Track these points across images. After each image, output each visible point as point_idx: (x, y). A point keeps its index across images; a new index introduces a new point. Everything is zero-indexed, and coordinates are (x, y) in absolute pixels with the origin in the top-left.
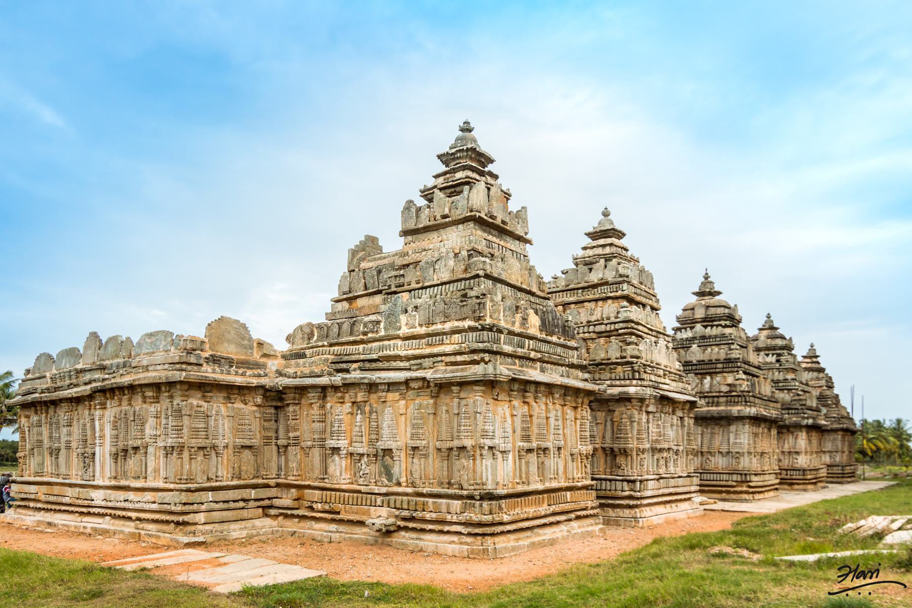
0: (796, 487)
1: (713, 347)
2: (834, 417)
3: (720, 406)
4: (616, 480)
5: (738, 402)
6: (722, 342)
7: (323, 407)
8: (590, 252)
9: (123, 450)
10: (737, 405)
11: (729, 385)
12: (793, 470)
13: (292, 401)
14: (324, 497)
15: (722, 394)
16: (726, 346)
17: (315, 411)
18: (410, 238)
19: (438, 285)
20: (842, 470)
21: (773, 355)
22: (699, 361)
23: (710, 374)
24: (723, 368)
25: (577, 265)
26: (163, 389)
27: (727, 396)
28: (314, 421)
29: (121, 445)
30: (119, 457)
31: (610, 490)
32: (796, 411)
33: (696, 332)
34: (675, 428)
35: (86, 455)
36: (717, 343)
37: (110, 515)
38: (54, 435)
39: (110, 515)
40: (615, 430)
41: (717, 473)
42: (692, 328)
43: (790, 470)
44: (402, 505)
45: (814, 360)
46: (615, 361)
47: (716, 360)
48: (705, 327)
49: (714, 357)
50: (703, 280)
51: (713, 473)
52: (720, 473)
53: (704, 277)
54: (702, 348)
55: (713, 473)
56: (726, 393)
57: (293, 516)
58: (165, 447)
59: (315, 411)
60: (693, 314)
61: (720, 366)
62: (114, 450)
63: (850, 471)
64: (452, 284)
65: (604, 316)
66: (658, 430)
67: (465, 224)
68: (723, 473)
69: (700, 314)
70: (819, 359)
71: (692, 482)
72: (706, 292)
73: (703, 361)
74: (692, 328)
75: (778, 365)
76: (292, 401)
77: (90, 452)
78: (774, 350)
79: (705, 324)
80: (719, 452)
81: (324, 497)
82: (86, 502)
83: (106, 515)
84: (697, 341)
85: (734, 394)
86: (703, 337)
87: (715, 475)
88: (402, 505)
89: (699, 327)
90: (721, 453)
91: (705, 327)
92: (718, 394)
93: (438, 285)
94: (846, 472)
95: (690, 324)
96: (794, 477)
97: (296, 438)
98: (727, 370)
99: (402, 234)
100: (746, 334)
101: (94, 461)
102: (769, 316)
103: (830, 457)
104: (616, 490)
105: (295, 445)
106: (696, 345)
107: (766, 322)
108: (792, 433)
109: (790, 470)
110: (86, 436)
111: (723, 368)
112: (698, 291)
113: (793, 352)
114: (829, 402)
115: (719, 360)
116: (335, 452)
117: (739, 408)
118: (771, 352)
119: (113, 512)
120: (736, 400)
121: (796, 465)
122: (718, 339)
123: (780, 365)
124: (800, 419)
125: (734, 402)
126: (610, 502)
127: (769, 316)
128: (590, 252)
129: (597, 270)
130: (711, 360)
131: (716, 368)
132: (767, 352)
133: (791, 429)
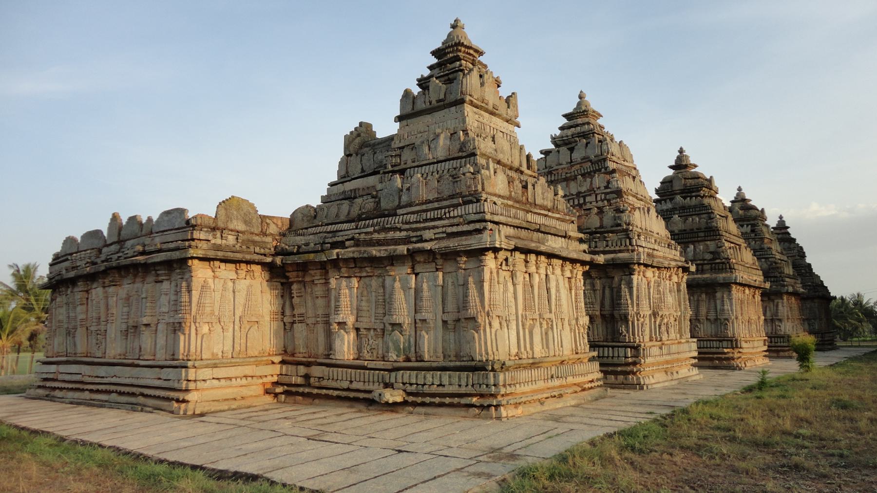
0: (782, 354)
1: (694, 217)
2: (810, 286)
3: (705, 274)
4: (619, 347)
5: (722, 269)
6: (701, 212)
7: (327, 283)
8: (569, 132)
9: (133, 326)
10: (722, 273)
11: (711, 253)
12: (778, 337)
13: (296, 279)
14: (331, 373)
15: (706, 262)
16: (706, 215)
17: (319, 290)
18: (404, 122)
19: (434, 163)
20: (822, 337)
21: (747, 225)
22: (680, 231)
23: (693, 243)
24: (705, 236)
25: (556, 145)
26: (175, 265)
27: (711, 264)
28: (317, 297)
29: (131, 323)
30: (129, 335)
31: (608, 357)
32: (775, 279)
33: (676, 203)
34: (673, 294)
35: (98, 332)
36: (697, 213)
37: (116, 392)
38: (71, 315)
39: (116, 392)
40: (615, 297)
41: (706, 341)
42: (671, 200)
43: (774, 337)
44: (410, 379)
45: (783, 231)
46: (609, 229)
47: (697, 229)
48: (685, 198)
49: (695, 227)
50: (679, 154)
51: (703, 341)
52: (710, 340)
53: (679, 151)
54: (683, 218)
55: (703, 341)
56: (710, 260)
57: (297, 394)
58: (174, 323)
59: (319, 290)
60: (672, 186)
61: (702, 234)
62: (124, 327)
63: (829, 338)
64: (448, 162)
65: (594, 186)
66: (659, 296)
67: (458, 106)
68: (713, 341)
69: (677, 186)
70: (789, 230)
71: (690, 347)
72: (681, 165)
73: (685, 230)
74: (671, 200)
75: (753, 235)
76: (296, 279)
77: (103, 329)
78: (749, 221)
79: (684, 195)
80: (707, 319)
81: (331, 373)
82: (96, 379)
83: (113, 392)
84: (678, 212)
85: (718, 261)
86: (683, 208)
87: (705, 342)
88: (410, 379)
89: (678, 198)
90: (710, 320)
91: (685, 198)
92: (702, 262)
93: (434, 163)
94: (826, 339)
95: (669, 195)
96: (779, 344)
97: (301, 315)
98: (709, 238)
99: (397, 119)
100: (723, 204)
101: (106, 338)
102: (740, 189)
103: (809, 324)
104: (618, 357)
105: (301, 322)
106: (677, 216)
107: (738, 195)
108: (773, 301)
109: (774, 337)
110: (99, 313)
111: (705, 236)
112: (674, 164)
113: (766, 222)
114: (803, 271)
115: (701, 229)
116: (342, 326)
117: (724, 275)
118: (746, 223)
119: (119, 388)
120: (720, 267)
121: (779, 333)
122: (697, 209)
123: (756, 235)
124: (779, 287)
125: (719, 269)
126: (783, 348)
127: (740, 189)
128: (569, 132)
129: (579, 149)
130: (692, 230)
131: (698, 237)
132: (741, 223)
133: (773, 297)
